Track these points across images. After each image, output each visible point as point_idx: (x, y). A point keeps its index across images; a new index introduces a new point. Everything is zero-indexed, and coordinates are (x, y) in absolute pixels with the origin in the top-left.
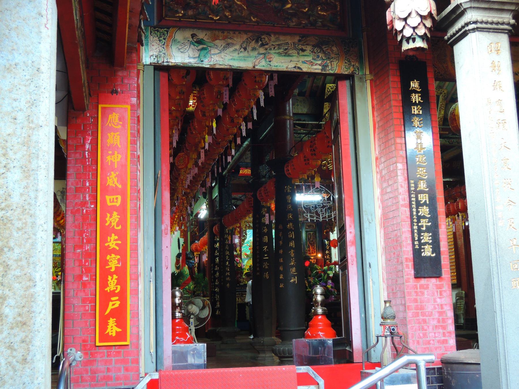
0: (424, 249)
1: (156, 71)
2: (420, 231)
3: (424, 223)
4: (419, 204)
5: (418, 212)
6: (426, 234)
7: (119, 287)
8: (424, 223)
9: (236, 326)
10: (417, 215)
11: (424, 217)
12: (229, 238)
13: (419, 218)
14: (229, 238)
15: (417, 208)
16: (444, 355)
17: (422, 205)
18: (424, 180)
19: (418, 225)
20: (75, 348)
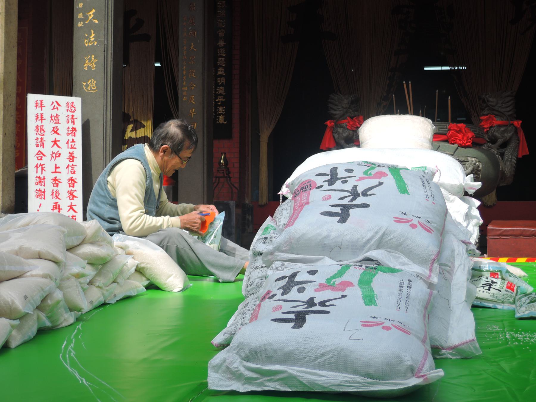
0: (219, 118)
1: (216, 142)
2: (216, 105)
3: (220, 99)
4: (217, 85)
5: (216, 91)
6: (221, 108)
7: (19, 144)
8: (220, 99)
9: (16, 172)
10: (215, 94)
11: (221, 95)
12: (140, 133)
13: (216, 96)
14: (140, 133)
15: (216, 88)
16: (138, 250)
17: (220, 86)
18: (223, 67)
19: (215, 101)
20: (331, 178)
